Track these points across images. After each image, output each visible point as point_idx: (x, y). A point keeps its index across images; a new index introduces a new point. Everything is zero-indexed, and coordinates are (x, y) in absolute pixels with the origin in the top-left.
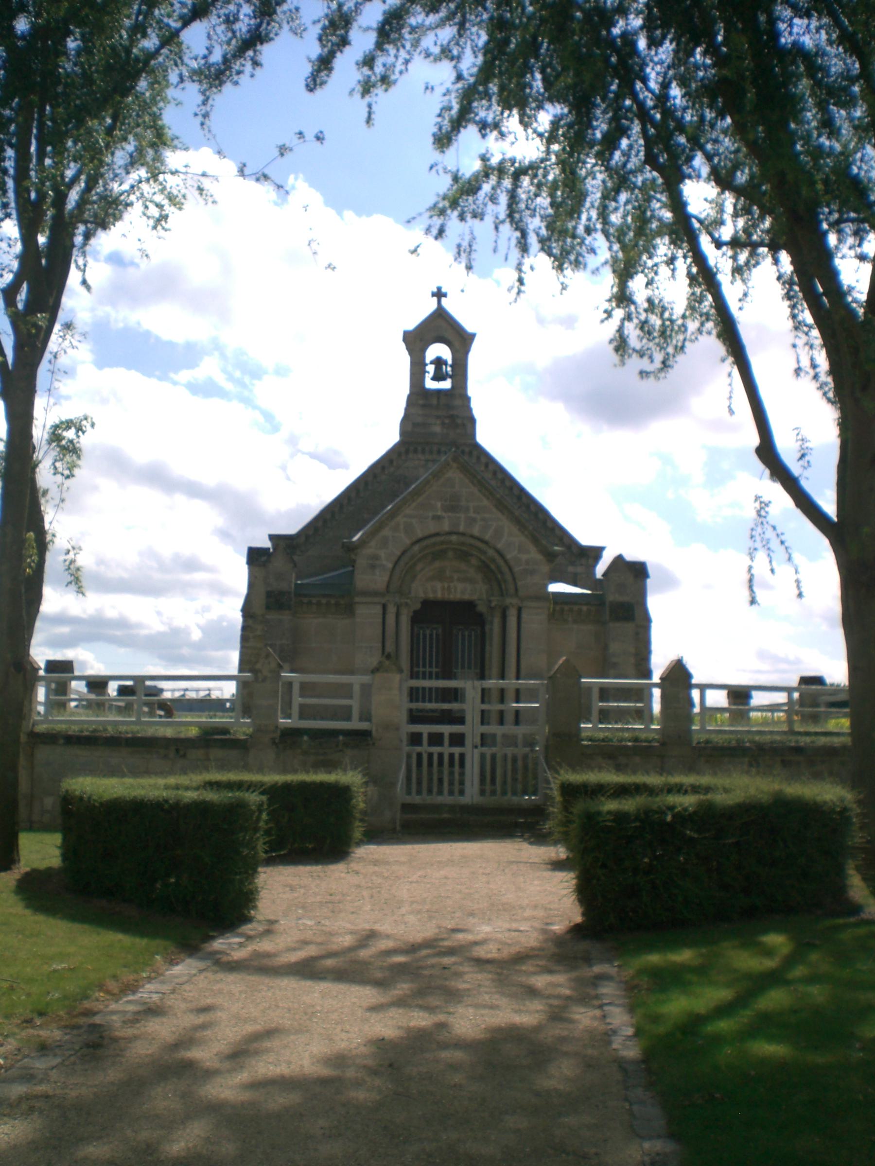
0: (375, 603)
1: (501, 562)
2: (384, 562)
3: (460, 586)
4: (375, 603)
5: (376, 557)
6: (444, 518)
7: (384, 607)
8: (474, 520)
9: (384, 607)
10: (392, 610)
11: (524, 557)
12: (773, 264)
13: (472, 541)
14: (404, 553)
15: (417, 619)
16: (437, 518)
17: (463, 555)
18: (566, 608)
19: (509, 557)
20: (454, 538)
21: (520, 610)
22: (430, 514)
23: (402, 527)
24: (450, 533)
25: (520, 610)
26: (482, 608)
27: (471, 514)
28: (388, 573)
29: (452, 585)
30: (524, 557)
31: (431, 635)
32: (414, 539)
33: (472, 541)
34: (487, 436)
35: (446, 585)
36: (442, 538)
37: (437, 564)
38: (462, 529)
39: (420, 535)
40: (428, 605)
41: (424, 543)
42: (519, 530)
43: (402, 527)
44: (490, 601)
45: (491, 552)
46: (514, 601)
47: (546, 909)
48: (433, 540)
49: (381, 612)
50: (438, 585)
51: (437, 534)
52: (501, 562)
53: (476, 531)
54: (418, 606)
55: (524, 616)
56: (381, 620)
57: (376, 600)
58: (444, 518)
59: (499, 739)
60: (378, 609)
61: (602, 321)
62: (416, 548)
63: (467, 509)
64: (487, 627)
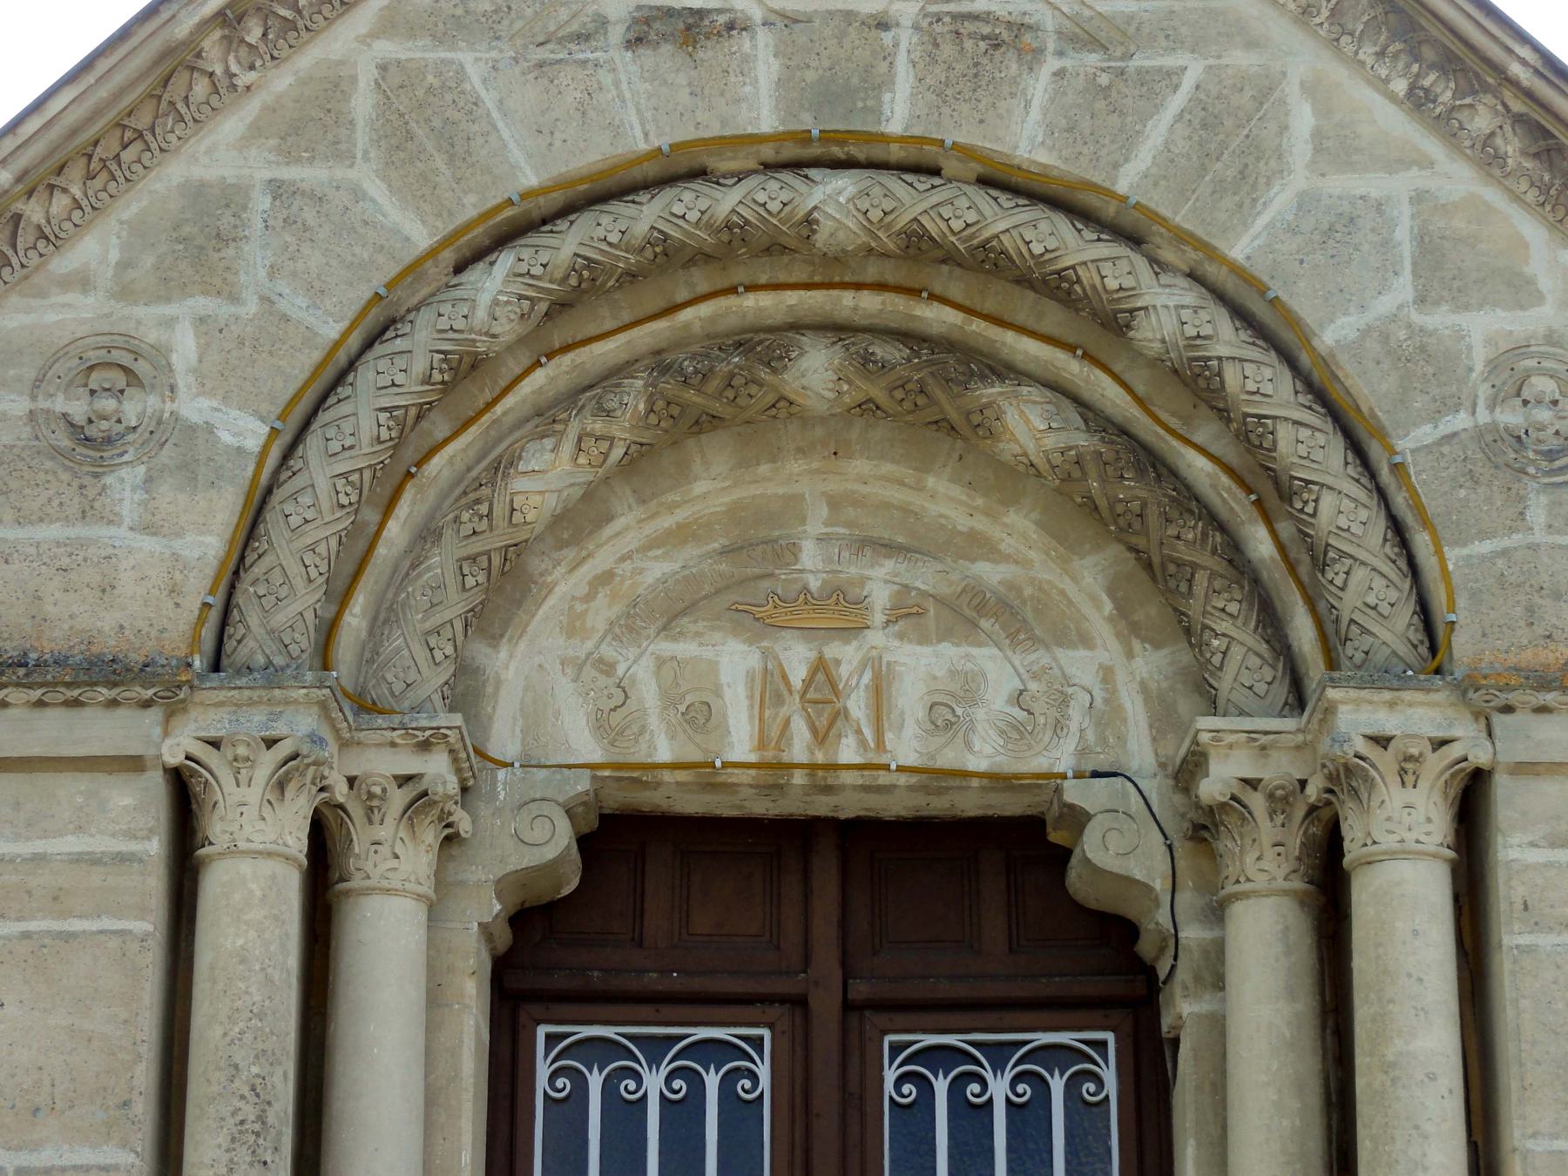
1: (1257, 382)
2: (193, 407)
3: (920, 666)
5: (119, 366)
7: (185, 798)
9: (185, 798)
11: (1481, 329)
13: (1001, 220)
14: (380, 327)
15: (543, 963)
17: (929, 395)
19: (1334, 333)
20: (834, 198)
21: (1471, 802)
23: (363, 104)
24: (798, 159)
25: (1471, 802)
26: (1120, 850)
28: (222, 511)
29: (847, 656)
30: (1481, 329)
31: (682, 1115)
32: (468, 207)
33: (1001, 220)
35: (797, 659)
36: (726, 202)
37: (713, 485)
38: (899, 113)
39: (526, 168)
40: (627, 839)
41: (568, 244)
42: (1418, 100)
43: (363, 104)
44: (1188, 770)
46: (1419, 715)
47: (1040, 589)
48: (645, 217)
49: (155, 847)
50: (733, 662)
51: (683, 169)
52: (1257, 382)
53: (1027, 135)
54: (549, 843)
55: (1515, 850)
56: (148, 925)
60: (133, 821)
62: (493, 283)
64: (1184, 1008)
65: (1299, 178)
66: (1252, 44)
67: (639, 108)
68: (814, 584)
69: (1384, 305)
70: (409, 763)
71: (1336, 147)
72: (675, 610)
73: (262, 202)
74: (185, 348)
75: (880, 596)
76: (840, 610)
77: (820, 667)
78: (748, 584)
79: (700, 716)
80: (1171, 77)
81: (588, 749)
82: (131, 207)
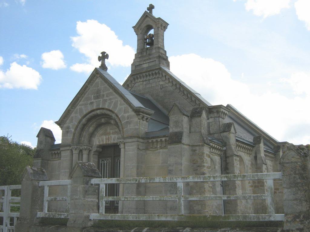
0: (68, 150)
2: (71, 129)
4: (68, 150)
6: (94, 102)
7: (72, 150)
8: (106, 101)
10: (75, 152)
11: (126, 115)
12: (162, 25)
16: (92, 103)
18: (154, 140)
22: (89, 102)
27: (105, 98)
29: (109, 136)
34: (135, 25)
45: (84, 120)
50: (104, 137)
57: (68, 148)
58: (94, 102)
59: (111, 199)
61: (151, 7)
63: (103, 95)
65: (119, 107)
66: (78, 110)
67: (90, 108)
68: (108, 132)
69: (122, 114)
70: (84, 147)
71: (121, 105)
72: (102, 135)
73: (74, 117)
74: (71, 126)
75: (111, 132)
76: (109, 134)
77: (108, 137)
78: (105, 134)
79: (103, 141)
80: (113, 101)
81: (98, 144)
82: (69, 119)
